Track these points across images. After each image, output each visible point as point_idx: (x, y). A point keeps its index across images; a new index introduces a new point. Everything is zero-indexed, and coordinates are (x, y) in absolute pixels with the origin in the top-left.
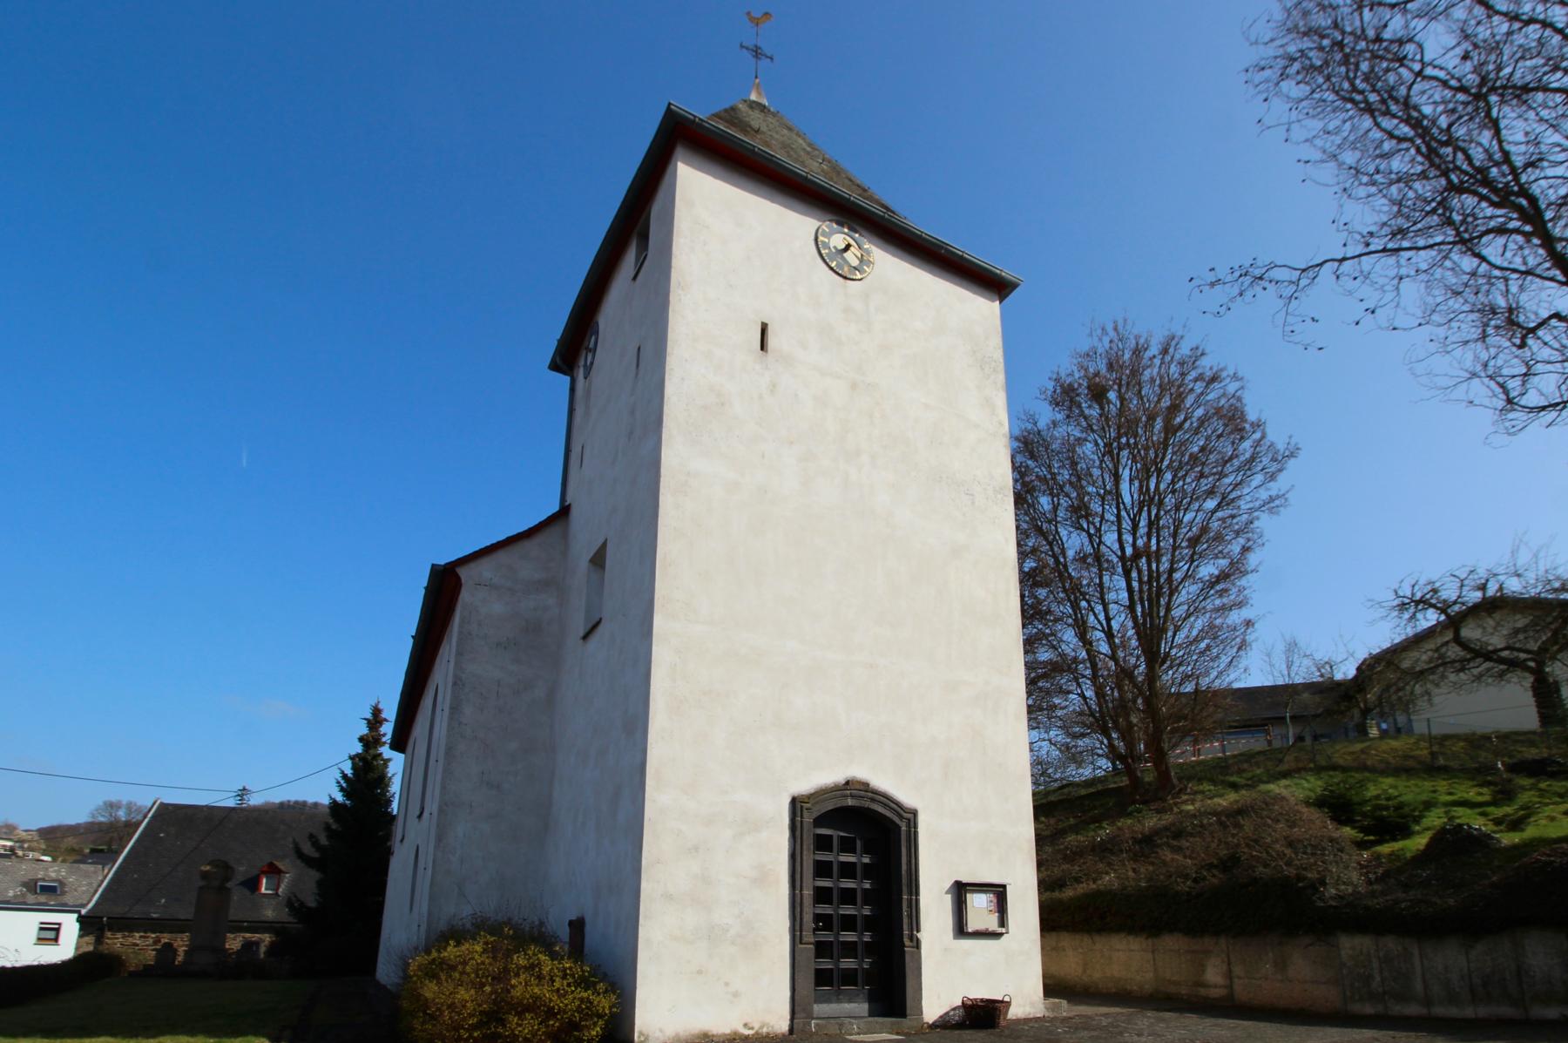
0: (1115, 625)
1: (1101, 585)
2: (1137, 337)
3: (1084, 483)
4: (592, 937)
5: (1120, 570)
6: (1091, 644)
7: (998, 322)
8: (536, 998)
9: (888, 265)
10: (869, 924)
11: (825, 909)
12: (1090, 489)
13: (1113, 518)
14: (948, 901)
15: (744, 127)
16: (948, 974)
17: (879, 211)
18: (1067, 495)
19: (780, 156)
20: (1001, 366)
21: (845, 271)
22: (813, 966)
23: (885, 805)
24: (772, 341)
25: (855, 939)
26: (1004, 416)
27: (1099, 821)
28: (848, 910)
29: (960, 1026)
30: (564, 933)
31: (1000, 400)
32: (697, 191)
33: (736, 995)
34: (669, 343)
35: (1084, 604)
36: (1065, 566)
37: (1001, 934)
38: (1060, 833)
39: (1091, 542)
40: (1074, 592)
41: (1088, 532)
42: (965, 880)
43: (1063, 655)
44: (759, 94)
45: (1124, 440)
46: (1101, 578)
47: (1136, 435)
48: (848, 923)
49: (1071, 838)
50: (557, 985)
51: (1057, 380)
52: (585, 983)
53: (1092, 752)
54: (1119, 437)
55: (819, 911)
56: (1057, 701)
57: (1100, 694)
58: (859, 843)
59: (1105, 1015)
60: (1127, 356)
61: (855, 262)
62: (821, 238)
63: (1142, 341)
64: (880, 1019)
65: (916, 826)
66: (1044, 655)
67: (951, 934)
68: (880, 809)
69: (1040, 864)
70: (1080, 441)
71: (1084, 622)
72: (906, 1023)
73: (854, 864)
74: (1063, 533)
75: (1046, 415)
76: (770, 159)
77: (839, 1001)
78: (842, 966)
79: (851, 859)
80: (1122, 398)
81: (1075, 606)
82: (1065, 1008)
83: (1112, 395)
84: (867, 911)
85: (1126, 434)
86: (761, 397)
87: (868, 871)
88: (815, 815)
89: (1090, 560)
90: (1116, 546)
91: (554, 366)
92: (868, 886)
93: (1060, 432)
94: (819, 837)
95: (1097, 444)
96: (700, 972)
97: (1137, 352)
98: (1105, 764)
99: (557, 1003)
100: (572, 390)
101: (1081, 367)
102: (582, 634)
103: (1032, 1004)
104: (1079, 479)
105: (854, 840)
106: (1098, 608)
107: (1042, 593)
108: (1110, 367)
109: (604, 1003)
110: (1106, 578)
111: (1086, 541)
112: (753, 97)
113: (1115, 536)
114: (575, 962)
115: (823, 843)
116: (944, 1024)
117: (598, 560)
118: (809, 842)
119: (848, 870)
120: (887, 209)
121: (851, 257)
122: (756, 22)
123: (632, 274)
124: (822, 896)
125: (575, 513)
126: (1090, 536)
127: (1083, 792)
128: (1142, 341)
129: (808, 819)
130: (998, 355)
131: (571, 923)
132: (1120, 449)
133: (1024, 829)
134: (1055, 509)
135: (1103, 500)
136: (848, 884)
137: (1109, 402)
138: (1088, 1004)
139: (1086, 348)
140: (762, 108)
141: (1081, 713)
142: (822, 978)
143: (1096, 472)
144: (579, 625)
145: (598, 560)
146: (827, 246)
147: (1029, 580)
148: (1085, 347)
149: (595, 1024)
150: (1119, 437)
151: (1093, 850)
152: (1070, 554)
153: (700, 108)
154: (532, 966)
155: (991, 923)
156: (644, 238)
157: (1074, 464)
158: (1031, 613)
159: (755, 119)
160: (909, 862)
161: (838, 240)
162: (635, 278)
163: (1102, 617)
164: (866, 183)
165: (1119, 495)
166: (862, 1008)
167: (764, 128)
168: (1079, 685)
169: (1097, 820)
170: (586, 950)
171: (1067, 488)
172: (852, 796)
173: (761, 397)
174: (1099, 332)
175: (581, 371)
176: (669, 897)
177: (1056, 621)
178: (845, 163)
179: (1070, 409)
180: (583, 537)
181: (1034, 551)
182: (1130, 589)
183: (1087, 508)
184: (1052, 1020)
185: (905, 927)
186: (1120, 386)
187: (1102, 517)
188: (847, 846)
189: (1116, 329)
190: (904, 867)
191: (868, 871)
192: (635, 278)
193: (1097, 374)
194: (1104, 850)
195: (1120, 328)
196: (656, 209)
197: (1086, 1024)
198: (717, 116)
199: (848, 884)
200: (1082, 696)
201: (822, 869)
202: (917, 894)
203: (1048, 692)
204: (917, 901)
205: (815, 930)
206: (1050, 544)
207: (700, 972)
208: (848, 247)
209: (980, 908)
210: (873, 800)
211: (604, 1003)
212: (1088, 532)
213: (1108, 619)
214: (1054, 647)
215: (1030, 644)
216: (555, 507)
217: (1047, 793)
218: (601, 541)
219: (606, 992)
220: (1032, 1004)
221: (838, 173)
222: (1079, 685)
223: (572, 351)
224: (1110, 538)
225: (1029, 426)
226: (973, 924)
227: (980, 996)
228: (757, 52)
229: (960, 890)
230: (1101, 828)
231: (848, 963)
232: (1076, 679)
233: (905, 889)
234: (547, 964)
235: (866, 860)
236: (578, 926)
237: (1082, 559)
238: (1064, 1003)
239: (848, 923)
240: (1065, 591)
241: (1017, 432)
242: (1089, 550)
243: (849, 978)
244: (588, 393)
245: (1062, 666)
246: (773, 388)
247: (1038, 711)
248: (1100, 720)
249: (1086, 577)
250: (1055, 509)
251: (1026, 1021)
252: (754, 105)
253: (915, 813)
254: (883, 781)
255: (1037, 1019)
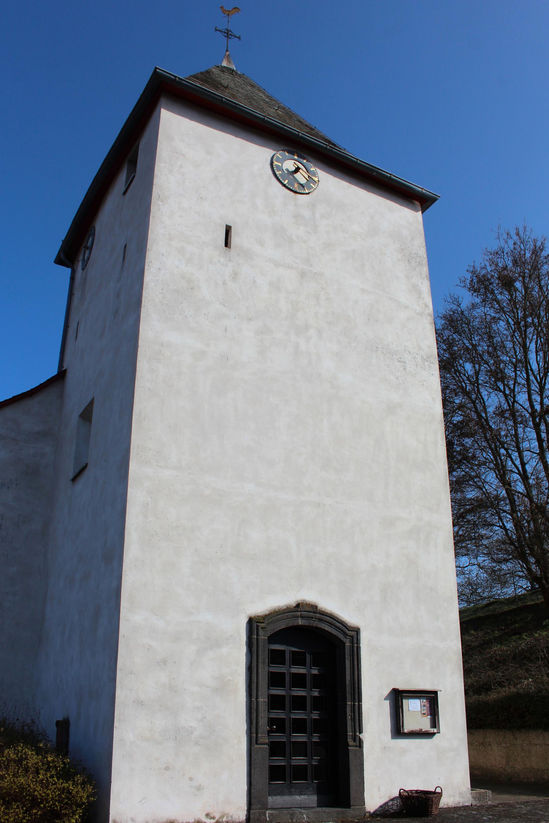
0: (529, 468)
1: (516, 435)
2: (535, 241)
3: (499, 353)
4: (75, 736)
5: (531, 423)
6: (509, 484)
7: (421, 227)
8: (22, 788)
9: (329, 183)
10: (317, 726)
11: (279, 714)
12: (505, 358)
13: (523, 382)
14: (387, 704)
15: (217, 85)
16: (387, 769)
17: (322, 143)
18: (486, 363)
19: (243, 104)
20: (425, 261)
21: (296, 187)
22: (267, 764)
23: (331, 624)
24: (234, 239)
25: (305, 739)
26: (428, 300)
27: (520, 634)
28: (299, 715)
29: (397, 815)
30: (52, 732)
31: (425, 287)
32: (178, 133)
33: (199, 788)
34: (149, 242)
35: (502, 451)
36: (487, 420)
37: (433, 734)
38: (485, 644)
39: (507, 400)
40: (494, 442)
41: (504, 392)
42: (401, 687)
43: (487, 494)
44: (229, 62)
45: (529, 320)
46: (516, 431)
47: (539, 317)
48: (299, 726)
49: (496, 648)
50: (41, 777)
51: (473, 272)
52: (66, 774)
53: (513, 574)
54: (525, 317)
55: (273, 716)
56: (483, 532)
57: (518, 524)
58: (308, 657)
59: (526, 803)
60: (528, 255)
61: (303, 181)
62: (275, 163)
63: (539, 244)
64: (327, 810)
65: (358, 642)
66: (471, 494)
67: (389, 735)
68: (327, 628)
69: (467, 672)
70: (495, 320)
71: (504, 467)
72: (350, 812)
73: (304, 675)
74: (484, 393)
75: (467, 299)
76: (235, 106)
77: (291, 794)
78: (294, 763)
79: (302, 671)
80: (526, 288)
81: (496, 454)
82: (490, 798)
83: (518, 285)
84: (315, 715)
85: (531, 315)
86: (224, 283)
87: (317, 681)
88: (269, 633)
89: (507, 415)
90: (527, 405)
91: (59, 261)
92: (316, 694)
93: (479, 312)
94: (273, 652)
95: (508, 323)
96: (167, 769)
97: (536, 252)
98: (525, 584)
99: (39, 791)
100: (72, 279)
101: (492, 262)
102: (71, 477)
103: (461, 794)
104: (495, 349)
105: (304, 654)
106: (515, 455)
107: (468, 441)
108: (515, 262)
109: (83, 795)
110: (520, 430)
111: (503, 400)
112: (224, 64)
113: (526, 396)
114: (57, 756)
115: (276, 657)
116: (383, 812)
117: (87, 415)
118: (264, 656)
119: (299, 681)
120: (330, 142)
121: (301, 177)
122: (228, 13)
123: (123, 189)
124: (275, 702)
125: (69, 376)
126: (506, 396)
127: (506, 608)
128: (539, 244)
129: (263, 637)
130: (422, 252)
131: (58, 723)
132: (526, 326)
133: (454, 644)
134: (477, 373)
135: (515, 367)
136: (299, 692)
137: (516, 290)
138: (510, 793)
139: (495, 248)
140: (231, 71)
141: (504, 543)
142: (276, 773)
143: (509, 345)
144: (69, 468)
145: (87, 415)
146: (280, 168)
147: (455, 433)
148: (494, 247)
149: (74, 813)
150: (525, 317)
151: (514, 658)
152: (491, 410)
153: (181, 70)
154: (21, 760)
155: (425, 724)
156: (133, 163)
157: (490, 337)
158: (456, 458)
159: (226, 79)
160: (353, 673)
161: (289, 165)
162: (125, 193)
163: (518, 462)
164: (313, 123)
165: (526, 362)
166: (312, 799)
167: (232, 85)
168: (500, 519)
169: (518, 632)
170: (70, 748)
171: (486, 357)
172: (302, 617)
173: (224, 283)
174: (505, 236)
175: (80, 264)
176: (140, 703)
177: (479, 465)
178: (295, 109)
179: (485, 294)
180: (75, 396)
181: (461, 407)
182: (540, 440)
183: (502, 372)
184: (478, 808)
185: (349, 728)
186: (524, 278)
187: (515, 382)
188: (298, 660)
189: (518, 234)
190: (348, 678)
191: (317, 681)
192: (125, 193)
193: (505, 268)
194: (524, 658)
195: (521, 233)
196: (143, 143)
197: (508, 811)
198: (195, 77)
199: (299, 692)
200: (504, 527)
201: (276, 680)
202: (360, 700)
203: (475, 525)
204: (360, 707)
205: (269, 732)
206: (474, 402)
207: (167, 769)
208: (297, 170)
209: (414, 712)
210: (320, 620)
211: (83, 795)
212: (504, 392)
213: (523, 464)
214: (480, 488)
215: (456, 486)
216: (54, 372)
217: (476, 610)
218: (90, 399)
219: (84, 783)
220: (461, 794)
221: (291, 117)
222: (500, 519)
223: (74, 249)
224: (522, 398)
225: (455, 307)
226: (408, 727)
227: (414, 788)
228: (228, 34)
229: (397, 697)
230: (520, 638)
231: (299, 760)
232: (498, 514)
233: (348, 696)
234: (33, 759)
235: (315, 672)
236: (63, 726)
237: (500, 413)
238: (489, 792)
239: (299, 726)
240: (487, 440)
241: (442, 312)
242: (506, 406)
243: (300, 773)
244: (84, 280)
245: (487, 503)
246: (235, 276)
247: (464, 541)
248: (519, 547)
249: (504, 428)
250: (477, 373)
251: (456, 809)
252: (224, 70)
253: (357, 631)
254: (329, 604)
255: (465, 808)
